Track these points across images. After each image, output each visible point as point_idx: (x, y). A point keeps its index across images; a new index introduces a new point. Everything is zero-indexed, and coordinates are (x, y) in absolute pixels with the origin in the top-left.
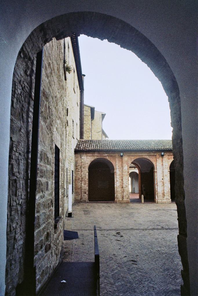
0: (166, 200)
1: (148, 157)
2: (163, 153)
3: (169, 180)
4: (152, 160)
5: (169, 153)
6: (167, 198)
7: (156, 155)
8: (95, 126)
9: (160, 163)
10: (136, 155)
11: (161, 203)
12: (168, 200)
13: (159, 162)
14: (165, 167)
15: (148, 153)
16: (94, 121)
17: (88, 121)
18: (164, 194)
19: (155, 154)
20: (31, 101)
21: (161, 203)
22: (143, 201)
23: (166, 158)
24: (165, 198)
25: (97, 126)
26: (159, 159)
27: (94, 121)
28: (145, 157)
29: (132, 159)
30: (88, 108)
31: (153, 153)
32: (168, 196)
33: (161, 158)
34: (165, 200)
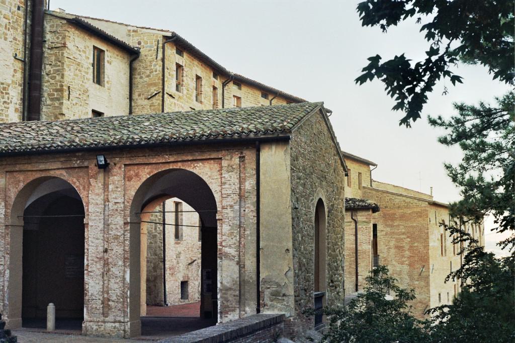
0: (113, 325)
1: (64, 172)
2: (101, 160)
3: (141, 252)
4: (75, 181)
5: (130, 158)
6: (118, 319)
7: (87, 167)
8: (141, 78)
9: (98, 194)
10: (29, 167)
11: (98, 336)
12: (117, 325)
13: (97, 191)
14: (115, 207)
15: (62, 159)
16: (141, 61)
17: (59, 63)
18: (105, 303)
19: (86, 164)
20: (514, 40)
21: (98, 336)
22: (51, 323)
23: (117, 177)
24: (111, 318)
25: (148, 76)
26: (96, 179)
27: (141, 61)
28: (57, 173)
29: (19, 181)
30: (59, 22)
31: (78, 158)
32: (119, 313)
33: (101, 176)
34: (109, 326)
